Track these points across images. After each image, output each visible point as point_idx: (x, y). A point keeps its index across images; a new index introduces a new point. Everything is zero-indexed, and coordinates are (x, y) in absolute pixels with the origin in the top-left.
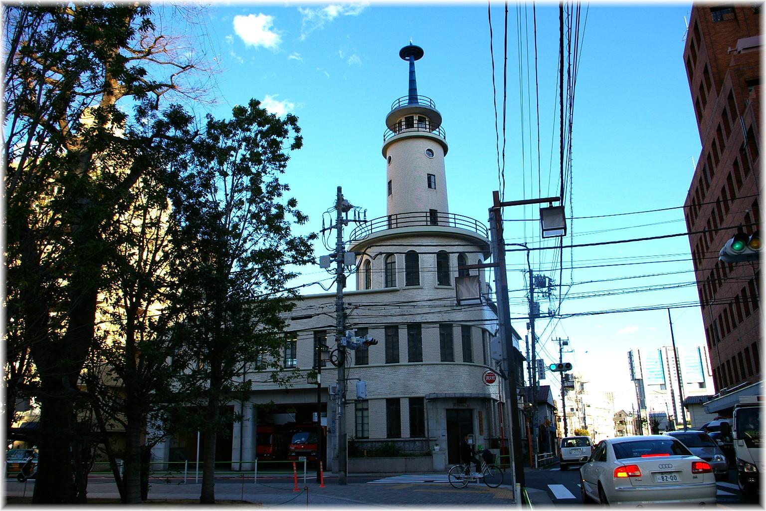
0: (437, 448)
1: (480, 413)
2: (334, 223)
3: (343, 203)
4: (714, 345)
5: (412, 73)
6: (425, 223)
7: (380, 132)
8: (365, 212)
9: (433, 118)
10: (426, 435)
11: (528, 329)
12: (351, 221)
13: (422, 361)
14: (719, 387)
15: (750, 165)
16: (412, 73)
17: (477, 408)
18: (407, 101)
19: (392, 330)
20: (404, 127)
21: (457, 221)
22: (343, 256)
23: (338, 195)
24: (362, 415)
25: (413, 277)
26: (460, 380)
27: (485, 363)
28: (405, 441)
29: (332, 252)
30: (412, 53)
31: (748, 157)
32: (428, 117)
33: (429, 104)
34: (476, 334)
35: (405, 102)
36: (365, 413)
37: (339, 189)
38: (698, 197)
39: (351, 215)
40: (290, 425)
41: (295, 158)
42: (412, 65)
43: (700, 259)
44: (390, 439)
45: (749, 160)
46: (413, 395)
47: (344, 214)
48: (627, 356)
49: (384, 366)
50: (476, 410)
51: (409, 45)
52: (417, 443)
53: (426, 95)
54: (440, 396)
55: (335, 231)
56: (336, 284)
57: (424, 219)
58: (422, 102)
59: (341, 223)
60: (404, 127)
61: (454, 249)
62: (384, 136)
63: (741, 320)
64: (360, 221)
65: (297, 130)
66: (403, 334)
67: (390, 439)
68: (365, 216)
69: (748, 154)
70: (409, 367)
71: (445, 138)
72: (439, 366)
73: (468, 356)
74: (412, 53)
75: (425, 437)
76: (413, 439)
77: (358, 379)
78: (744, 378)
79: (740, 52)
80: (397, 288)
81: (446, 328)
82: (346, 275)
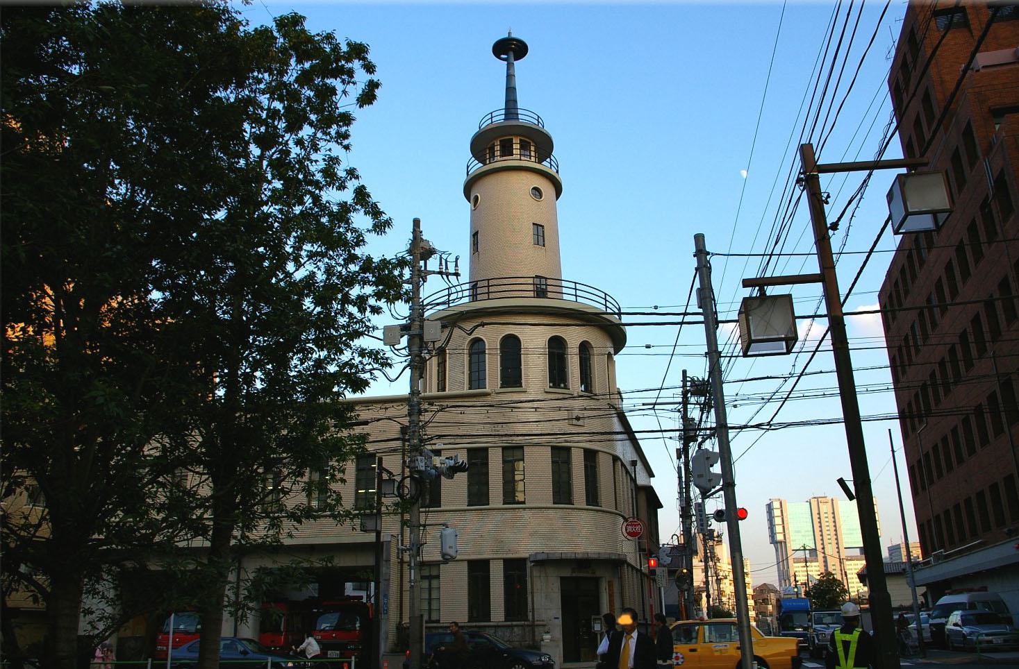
0: (547, 637)
1: (610, 584)
3: (422, 244)
4: (924, 488)
5: (510, 77)
7: (462, 162)
8: (457, 259)
9: (540, 143)
10: (530, 617)
11: (679, 458)
12: (434, 272)
13: (488, 504)
14: (930, 548)
15: (998, 227)
16: (510, 77)
17: (605, 578)
18: (503, 117)
21: (579, 293)
22: (422, 327)
23: (414, 232)
24: (430, 585)
25: (512, 376)
26: (583, 533)
27: (616, 509)
28: (496, 627)
29: (404, 322)
30: (511, 49)
31: (995, 215)
32: (533, 142)
34: (604, 464)
35: (499, 118)
36: (434, 583)
37: (416, 223)
38: (904, 280)
39: (433, 264)
40: (311, 602)
41: (364, 122)
42: (510, 66)
43: (903, 366)
44: (474, 624)
45: (997, 221)
46: (510, 556)
48: (764, 510)
49: (465, 510)
50: (604, 579)
51: (507, 36)
52: (516, 629)
53: (530, 108)
54: (551, 557)
56: (408, 371)
58: (525, 118)
61: (574, 336)
62: (468, 167)
63: (972, 451)
64: (448, 275)
65: (370, 68)
67: (474, 624)
68: (456, 265)
69: (994, 212)
71: (557, 172)
72: (550, 511)
73: (592, 497)
74: (511, 49)
75: (527, 620)
76: (509, 623)
77: (443, 525)
78: (975, 535)
79: (978, 71)
80: (487, 390)
81: (561, 455)
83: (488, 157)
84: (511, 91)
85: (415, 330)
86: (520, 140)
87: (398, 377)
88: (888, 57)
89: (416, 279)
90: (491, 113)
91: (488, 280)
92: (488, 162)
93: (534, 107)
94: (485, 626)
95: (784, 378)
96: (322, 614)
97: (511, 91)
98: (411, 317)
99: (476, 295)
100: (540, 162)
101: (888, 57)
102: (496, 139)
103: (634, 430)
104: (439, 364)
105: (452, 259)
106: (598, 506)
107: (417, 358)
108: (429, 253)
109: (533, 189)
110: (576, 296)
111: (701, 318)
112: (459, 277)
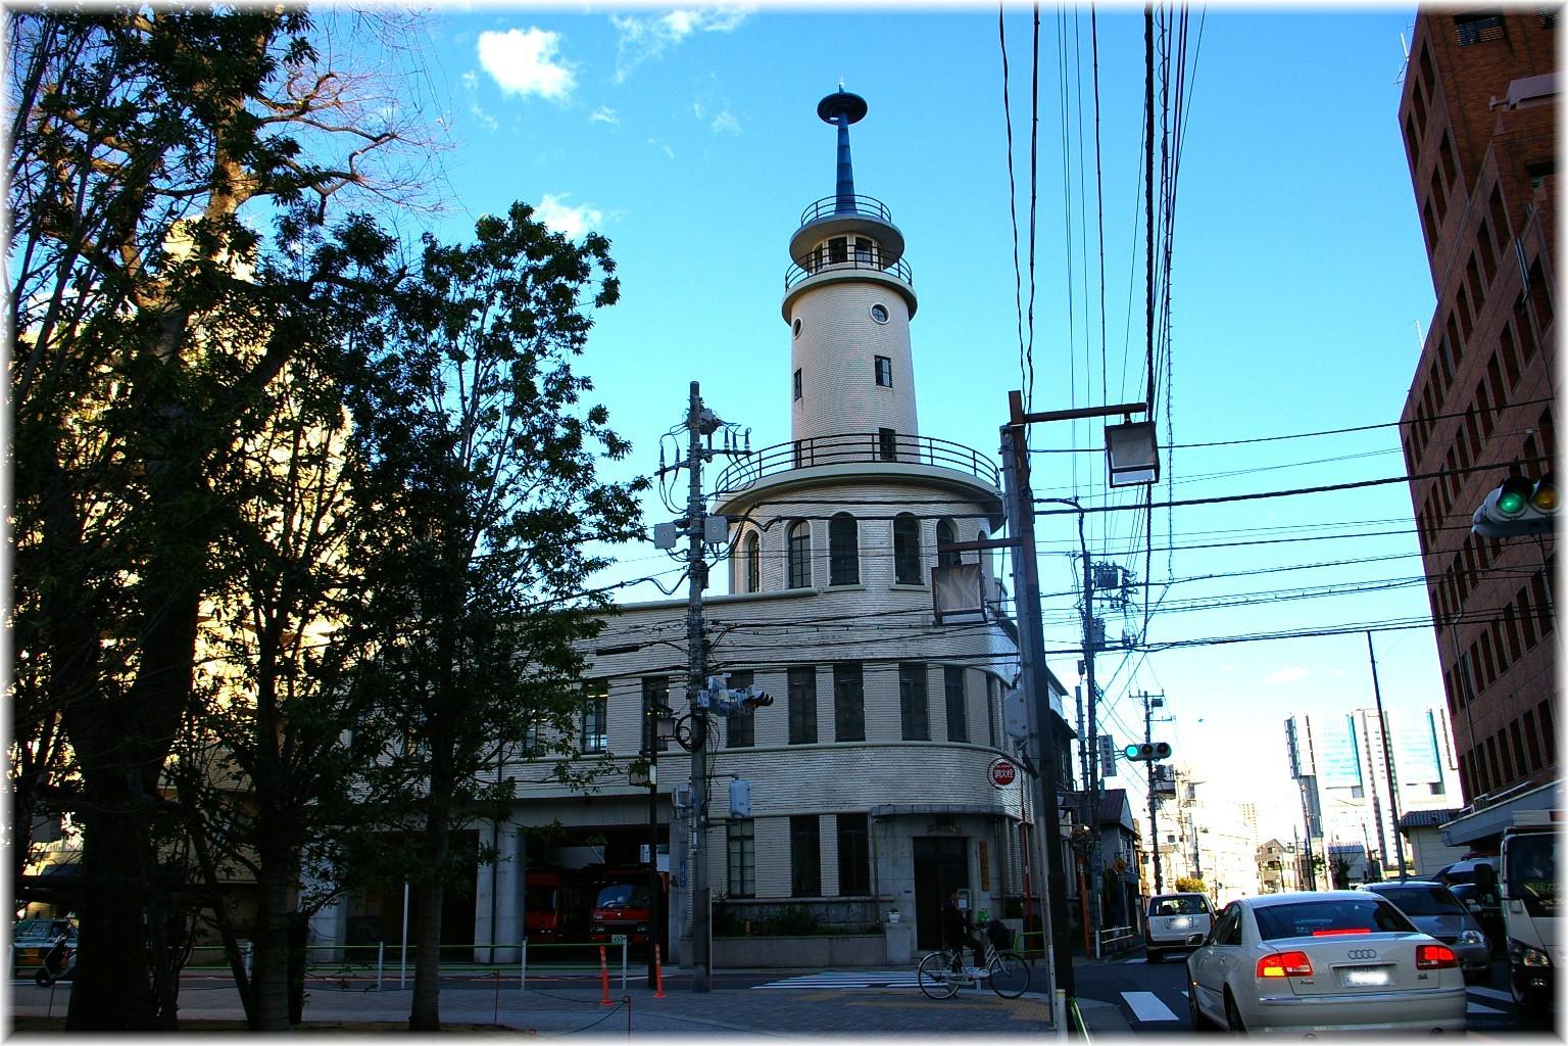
0: (894, 917)
1: (983, 846)
2: (684, 457)
3: (702, 415)
4: (1462, 706)
5: (843, 149)
6: (870, 457)
7: (779, 271)
9: (886, 242)
10: (873, 891)
11: (1081, 673)
12: (718, 452)
13: (864, 739)
14: (1473, 793)
15: (1535, 338)
16: (843, 149)
17: (976, 836)
18: (834, 207)
19: (802, 676)
20: (826, 260)
21: (935, 453)
22: (702, 524)
23: (692, 400)
24: (742, 849)
25: (845, 568)
26: (941, 779)
27: (993, 744)
28: (829, 903)
29: (680, 517)
30: (843, 109)
31: (1532, 321)
32: (877, 240)
34: (974, 684)
36: (748, 846)
37: (695, 387)
38: (1429, 404)
39: (718, 439)
40: (593, 870)
42: (843, 134)
43: (1432, 530)
44: (799, 900)
45: (1533, 329)
46: (846, 809)
47: (703, 439)
48: (1284, 728)
49: (786, 750)
50: (973, 840)
51: (837, 91)
52: (854, 906)
53: (873, 194)
54: (900, 811)
55: (685, 473)
56: (687, 580)
57: (869, 448)
58: (865, 208)
59: (698, 456)
60: (826, 260)
61: (930, 509)
62: (787, 279)
63: (1517, 655)
64: (736, 453)
65: (609, 266)
66: (825, 683)
67: (799, 900)
68: (747, 442)
71: (910, 283)
72: (899, 750)
73: (958, 730)
74: (843, 109)
75: (869, 894)
76: (845, 898)
77: (733, 776)
78: (1523, 773)
79: (1514, 107)
80: (813, 589)
81: (912, 672)
82: (709, 562)
89: (694, 461)
94: (813, 903)
96: (605, 886)
98: (688, 511)
110: (932, 457)
111: (1037, 507)
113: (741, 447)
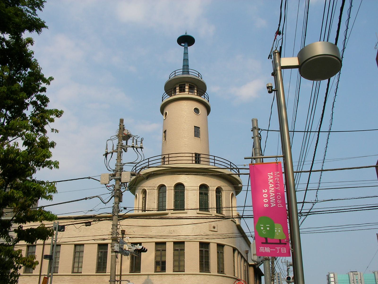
2: (115, 148)
5: (186, 54)
6: (191, 162)
7: (159, 95)
9: (199, 86)
13: (184, 271)
16: (186, 54)
19: (160, 246)
20: (178, 91)
21: (216, 162)
25: (179, 204)
33: (198, 76)
37: (122, 121)
47: (124, 142)
48: (326, 278)
55: (115, 154)
57: (191, 158)
58: (192, 74)
59: (121, 149)
60: (178, 91)
61: (213, 184)
62: (163, 98)
66: (170, 248)
70: (173, 276)
71: (208, 101)
74: (186, 40)
81: (204, 246)
82: (122, 190)
83: (173, 93)
84: (186, 60)
85: (117, 177)
86: (189, 85)
87: (108, 201)
88: (376, 48)
90: (175, 71)
91: (169, 154)
92: (173, 95)
93: (199, 68)
95: (312, 203)
97: (186, 60)
99: (164, 162)
100: (200, 96)
101: (376, 48)
102: (177, 84)
103: (245, 232)
104: (143, 198)
105: (139, 140)
106: (224, 274)
107: (118, 191)
108: (127, 137)
109: (194, 109)
112: (142, 149)
113: (139, 145)
